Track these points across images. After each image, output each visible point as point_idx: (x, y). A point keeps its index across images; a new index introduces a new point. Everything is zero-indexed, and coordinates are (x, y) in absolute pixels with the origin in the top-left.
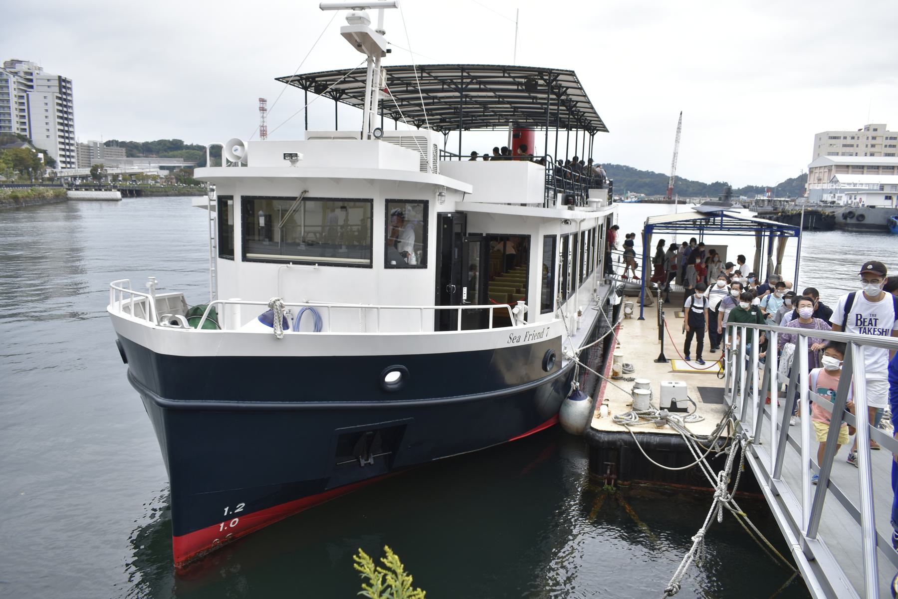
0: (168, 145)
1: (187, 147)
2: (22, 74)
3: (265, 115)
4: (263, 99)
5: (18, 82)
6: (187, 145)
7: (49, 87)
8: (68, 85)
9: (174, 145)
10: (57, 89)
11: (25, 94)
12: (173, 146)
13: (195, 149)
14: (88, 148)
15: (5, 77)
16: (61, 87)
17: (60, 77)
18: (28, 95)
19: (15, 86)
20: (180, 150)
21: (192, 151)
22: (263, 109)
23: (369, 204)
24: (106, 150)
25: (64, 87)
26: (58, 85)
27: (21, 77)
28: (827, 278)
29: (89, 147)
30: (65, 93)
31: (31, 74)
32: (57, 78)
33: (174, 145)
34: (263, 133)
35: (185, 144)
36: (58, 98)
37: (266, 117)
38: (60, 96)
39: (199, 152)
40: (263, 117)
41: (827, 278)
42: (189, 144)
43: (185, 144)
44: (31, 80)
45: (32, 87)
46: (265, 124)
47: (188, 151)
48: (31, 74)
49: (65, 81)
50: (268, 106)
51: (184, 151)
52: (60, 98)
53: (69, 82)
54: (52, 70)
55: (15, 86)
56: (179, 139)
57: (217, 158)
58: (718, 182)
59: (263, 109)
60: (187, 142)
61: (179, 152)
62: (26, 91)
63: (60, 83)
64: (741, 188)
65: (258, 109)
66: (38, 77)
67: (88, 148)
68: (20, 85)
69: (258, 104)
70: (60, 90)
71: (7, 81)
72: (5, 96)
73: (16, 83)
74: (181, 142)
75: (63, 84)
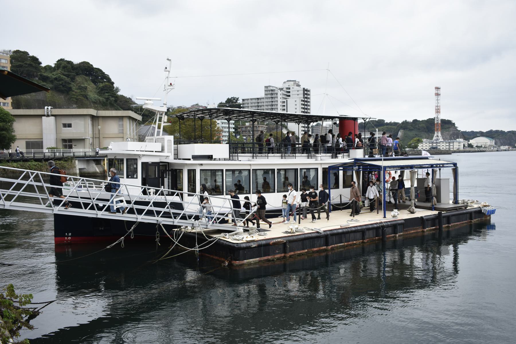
0: (375, 123)
1: (387, 124)
2: (285, 89)
3: (439, 98)
4: (438, 87)
5: (283, 94)
6: (387, 123)
7: (298, 95)
8: (308, 93)
9: (379, 123)
10: (302, 96)
11: (285, 101)
12: (378, 124)
13: (393, 125)
14: (326, 128)
15: (276, 92)
16: (304, 94)
17: (304, 88)
18: (287, 101)
19: (281, 96)
20: (382, 126)
21: (390, 126)
22: (438, 95)
23: (129, 160)
24: (336, 129)
25: (306, 94)
26: (303, 93)
27: (284, 91)
28: (146, 331)
29: (326, 128)
30: (306, 98)
31: (289, 89)
32: (303, 89)
33: (379, 123)
34: (438, 111)
35: (386, 122)
36: (302, 101)
37: (440, 100)
38: (304, 99)
39: (395, 127)
40: (438, 100)
41: (146, 331)
42: (388, 122)
43: (386, 122)
44: (289, 92)
45: (289, 96)
46: (439, 105)
47: (388, 126)
48: (289, 89)
49: (306, 90)
50: (441, 92)
51: (385, 126)
52: (303, 101)
53: (309, 91)
54: (304, 85)
55: (281, 96)
56: (382, 119)
57: (405, 130)
58: (406, 121)
59: (438, 95)
60: (387, 121)
61: (382, 127)
62: (286, 98)
63: (304, 92)
64: (467, 131)
65: (434, 94)
66: (293, 90)
67: (326, 128)
68: (283, 95)
69: (434, 91)
70: (304, 96)
71: (277, 94)
72: (276, 102)
73: (282, 95)
74: (383, 121)
75: (306, 92)
